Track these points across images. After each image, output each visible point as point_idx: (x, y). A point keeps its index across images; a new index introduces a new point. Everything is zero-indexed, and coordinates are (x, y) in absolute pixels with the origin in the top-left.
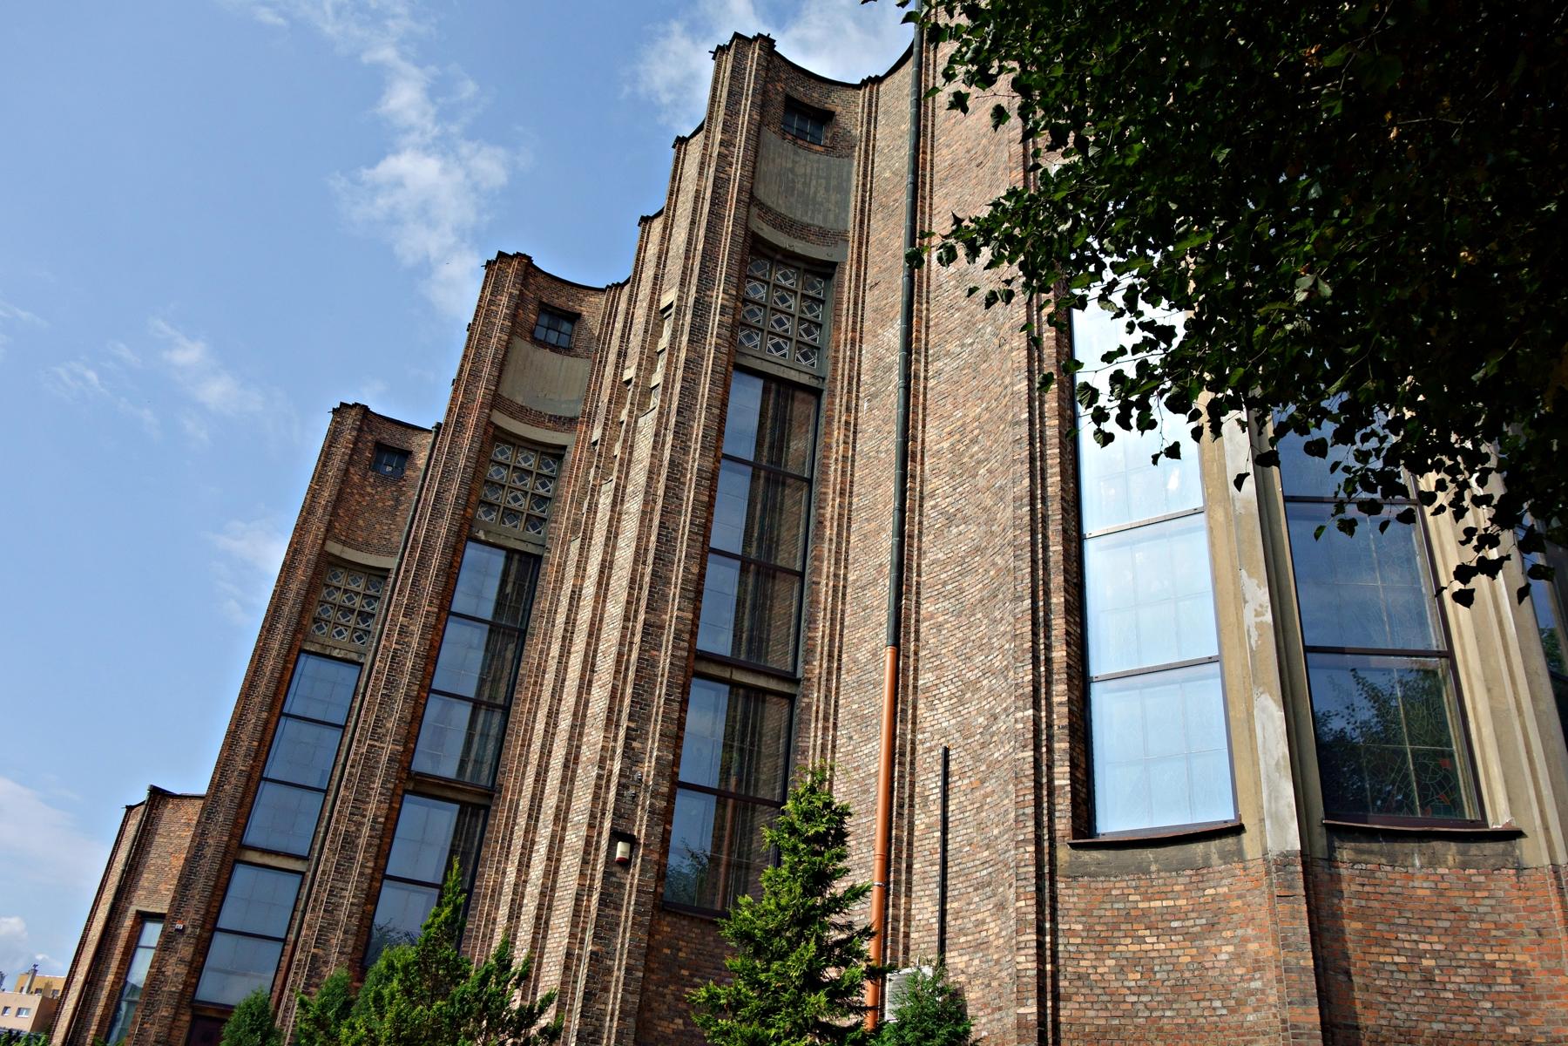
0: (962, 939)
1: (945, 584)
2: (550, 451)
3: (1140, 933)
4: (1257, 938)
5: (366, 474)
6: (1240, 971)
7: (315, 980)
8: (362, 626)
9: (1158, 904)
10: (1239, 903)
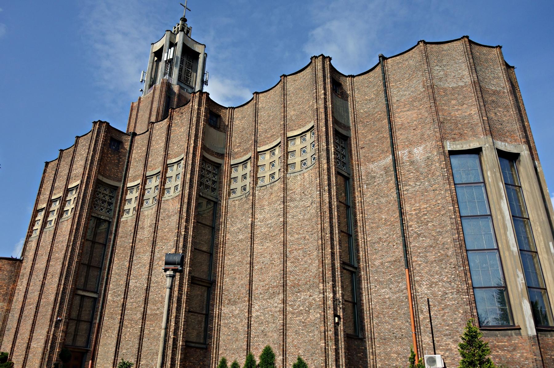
0: (441, 348)
1: (419, 253)
2: (216, 165)
3: (497, 350)
4: (526, 353)
5: (108, 149)
6: (522, 359)
7: (175, 346)
8: (109, 207)
9: (500, 344)
10: (521, 345)
